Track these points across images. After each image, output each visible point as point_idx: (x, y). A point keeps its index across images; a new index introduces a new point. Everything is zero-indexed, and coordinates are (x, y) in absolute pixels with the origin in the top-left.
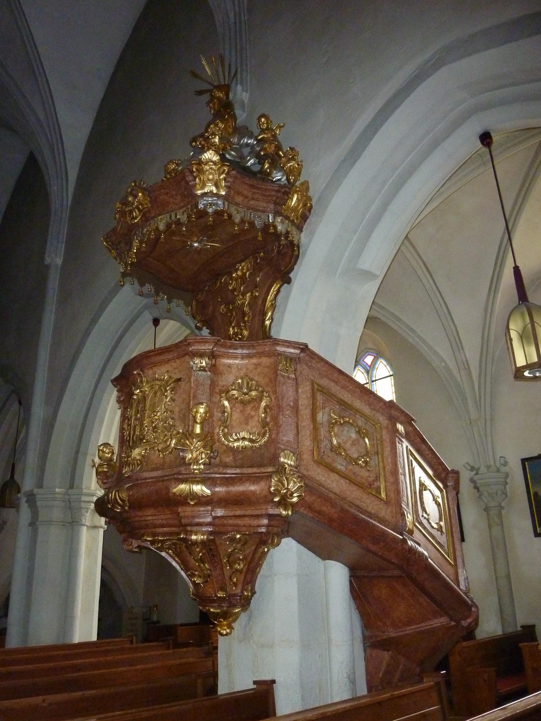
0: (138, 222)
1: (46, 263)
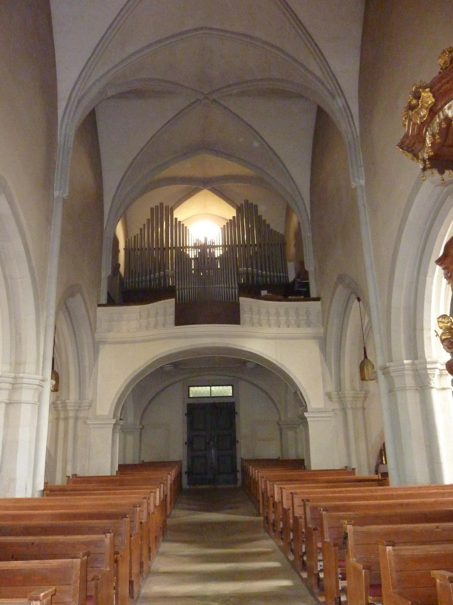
0: (427, 119)
1: (353, 187)
